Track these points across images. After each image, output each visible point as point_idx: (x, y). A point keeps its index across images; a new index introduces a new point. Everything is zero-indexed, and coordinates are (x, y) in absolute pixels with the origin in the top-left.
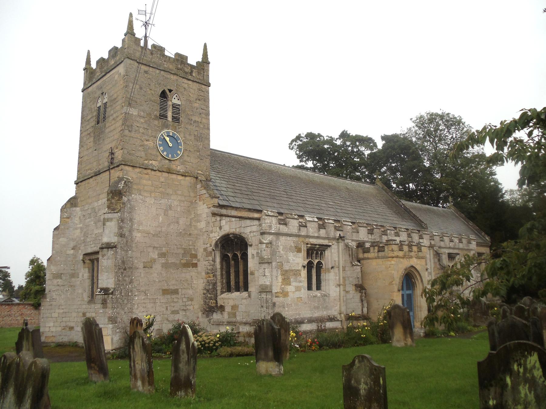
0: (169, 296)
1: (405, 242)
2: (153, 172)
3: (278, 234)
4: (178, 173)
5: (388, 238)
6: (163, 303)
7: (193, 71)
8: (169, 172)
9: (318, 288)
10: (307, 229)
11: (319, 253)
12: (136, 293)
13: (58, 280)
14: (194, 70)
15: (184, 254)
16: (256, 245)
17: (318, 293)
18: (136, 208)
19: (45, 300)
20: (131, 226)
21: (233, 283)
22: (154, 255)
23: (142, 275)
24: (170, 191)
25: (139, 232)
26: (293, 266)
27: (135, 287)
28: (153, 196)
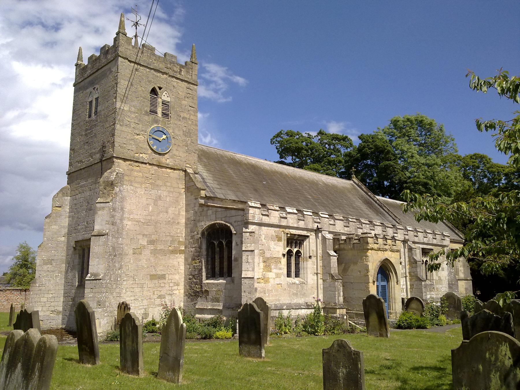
0: (156, 281)
1: (380, 235)
2: (144, 165)
3: (260, 224)
4: (167, 166)
5: (363, 231)
6: (150, 287)
7: (182, 70)
8: (159, 166)
9: (297, 275)
10: (288, 220)
11: (298, 242)
12: (125, 279)
13: (48, 266)
14: (182, 69)
15: (173, 241)
16: (240, 234)
17: (296, 280)
18: (127, 198)
19: (34, 285)
20: (122, 216)
21: (217, 269)
22: (144, 242)
23: (132, 262)
24: (159, 182)
25: (129, 220)
26: (274, 254)
27: (124, 273)
28: (143, 186)
